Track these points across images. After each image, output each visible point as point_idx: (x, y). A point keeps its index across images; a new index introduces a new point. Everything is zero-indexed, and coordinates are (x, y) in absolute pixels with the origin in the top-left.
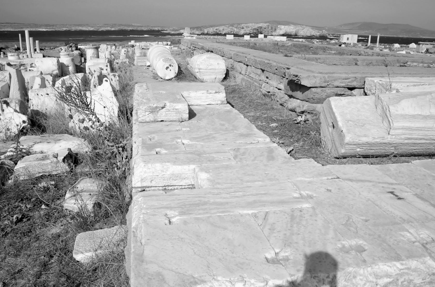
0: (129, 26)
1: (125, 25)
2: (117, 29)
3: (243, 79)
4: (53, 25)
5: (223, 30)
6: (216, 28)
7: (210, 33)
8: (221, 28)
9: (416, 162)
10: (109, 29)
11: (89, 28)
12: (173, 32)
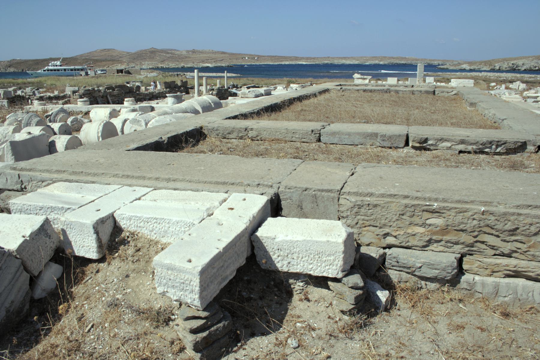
0: (402, 58)
1: (397, 58)
2: (386, 63)
3: (303, 353)
4: (314, 58)
5: (523, 64)
6: (512, 62)
7: (504, 69)
8: (520, 63)
9: (85, 203)
10: (377, 62)
11: (354, 61)
12: (451, 68)
